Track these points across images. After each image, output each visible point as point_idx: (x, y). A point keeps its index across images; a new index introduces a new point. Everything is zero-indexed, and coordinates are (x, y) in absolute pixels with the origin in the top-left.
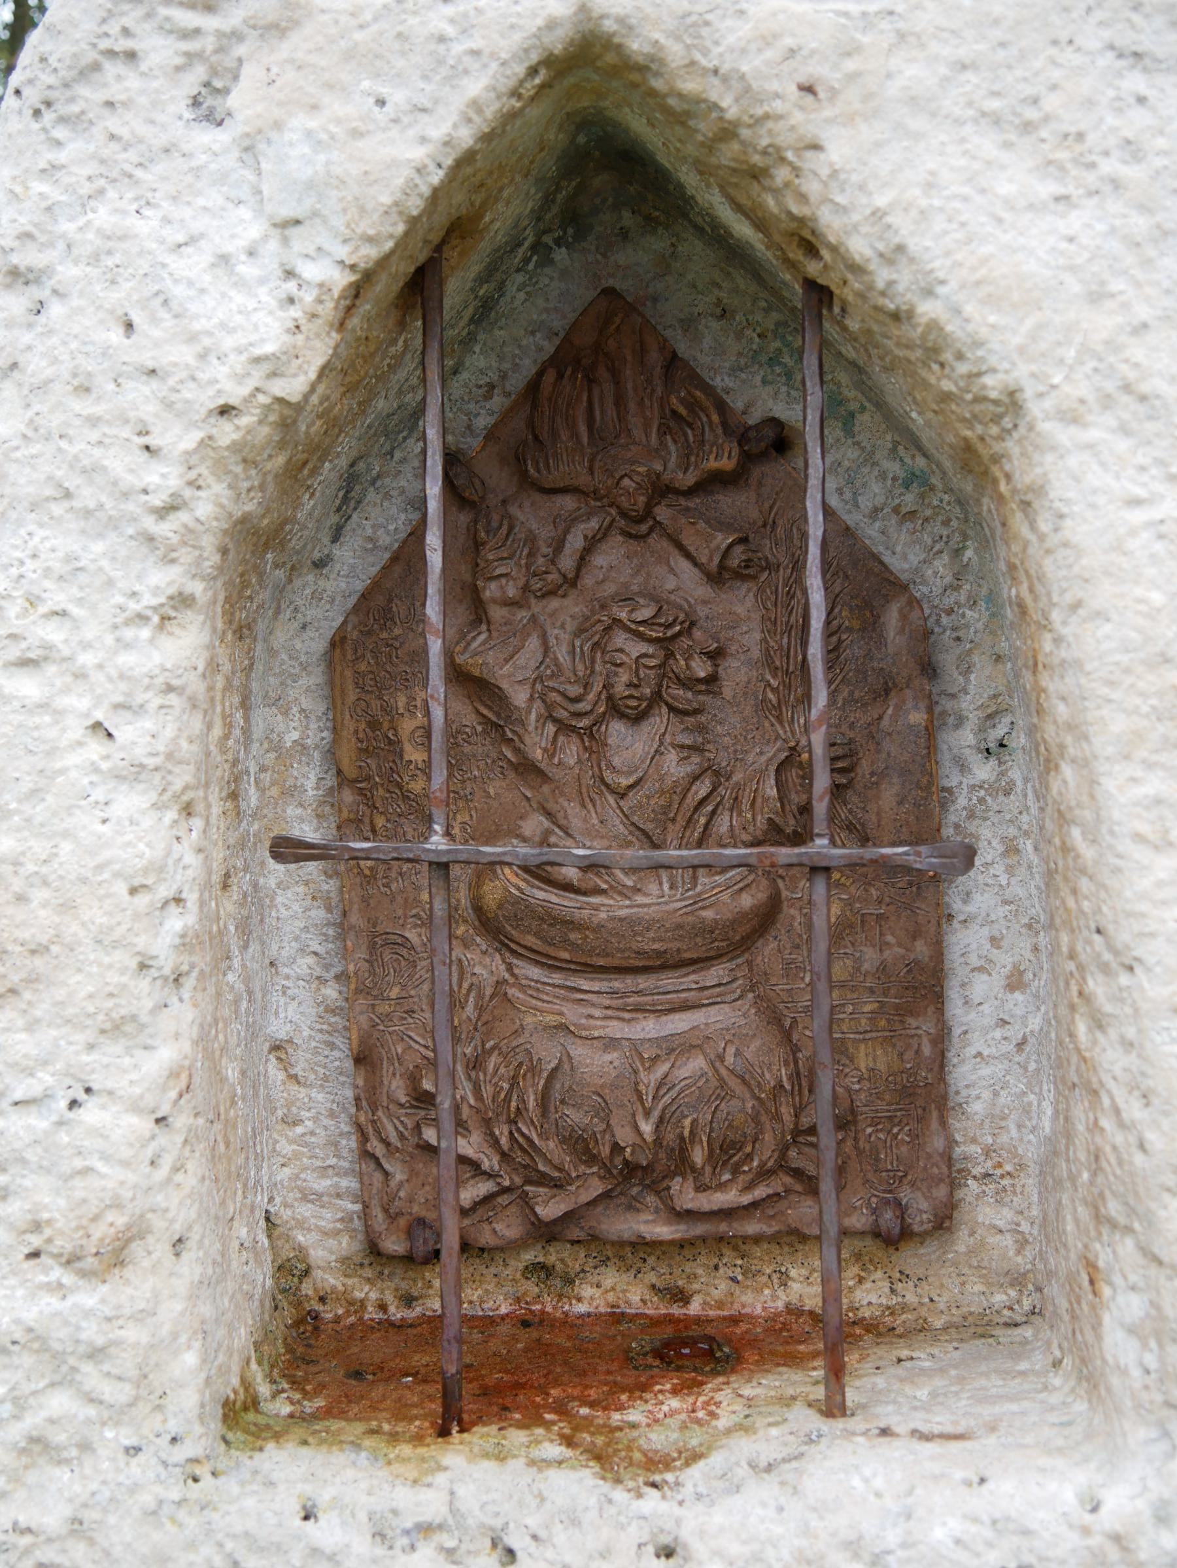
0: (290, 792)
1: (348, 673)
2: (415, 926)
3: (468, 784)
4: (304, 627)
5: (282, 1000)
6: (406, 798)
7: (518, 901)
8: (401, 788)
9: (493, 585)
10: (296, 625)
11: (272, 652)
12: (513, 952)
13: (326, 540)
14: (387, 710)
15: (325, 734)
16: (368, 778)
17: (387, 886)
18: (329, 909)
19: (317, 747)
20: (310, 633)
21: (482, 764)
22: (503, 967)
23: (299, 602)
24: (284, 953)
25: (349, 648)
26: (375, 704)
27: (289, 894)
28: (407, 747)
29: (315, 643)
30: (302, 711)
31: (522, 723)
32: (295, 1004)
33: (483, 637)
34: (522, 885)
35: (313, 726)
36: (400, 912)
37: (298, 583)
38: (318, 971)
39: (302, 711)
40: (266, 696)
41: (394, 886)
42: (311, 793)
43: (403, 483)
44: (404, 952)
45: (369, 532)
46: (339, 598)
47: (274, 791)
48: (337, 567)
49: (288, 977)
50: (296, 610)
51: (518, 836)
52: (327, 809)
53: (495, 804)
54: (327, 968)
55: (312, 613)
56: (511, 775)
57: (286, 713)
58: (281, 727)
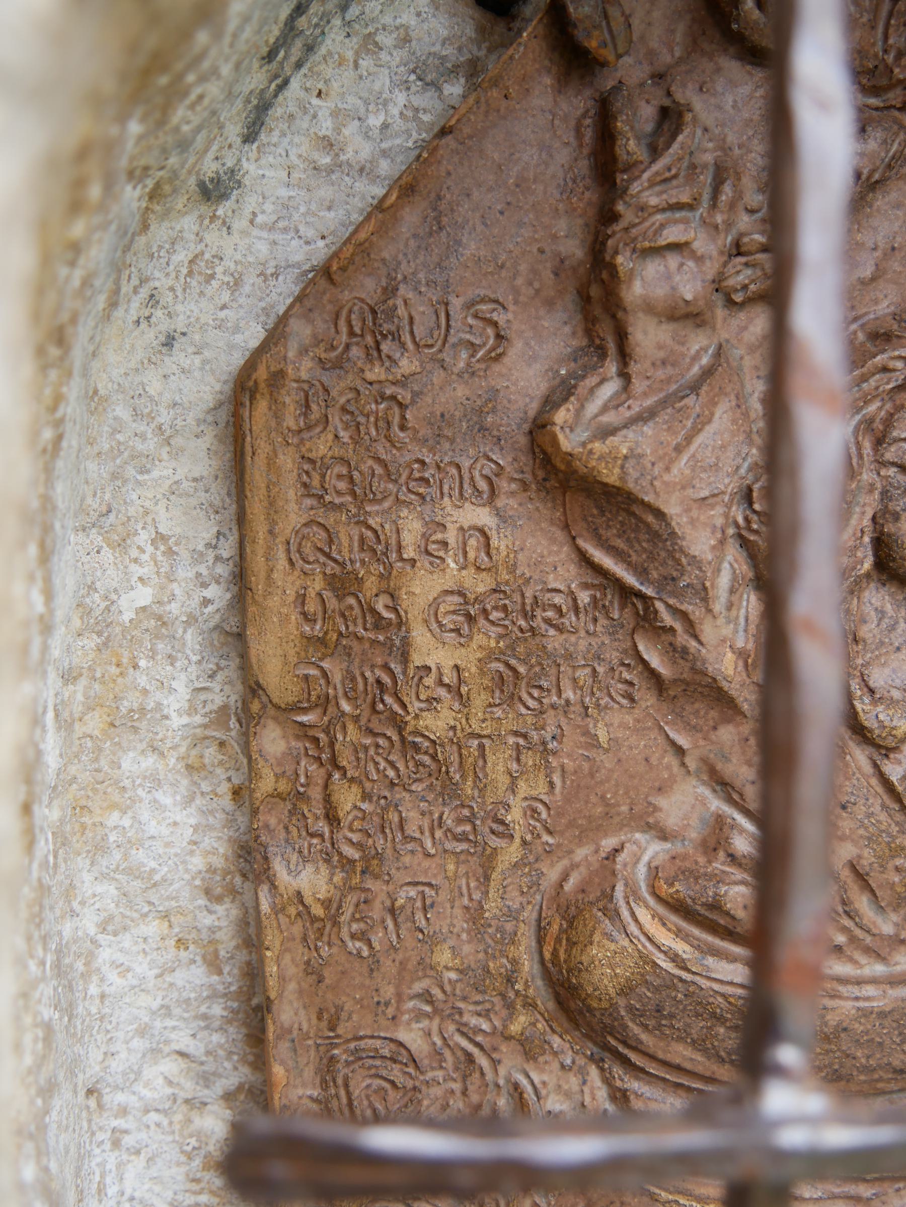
0: (126, 722)
1: (287, 461)
2: (419, 1015)
3: (550, 718)
4: (169, 342)
5: (112, 1159)
6: (408, 747)
7: (671, 982)
8: (400, 725)
9: (652, 268)
10: (151, 336)
11: (94, 399)
12: (626, 1062)
13: (234, 131)
14: (380, 549)
15: (214, 591)
16: (325, 703)
17: (361, 936)
18: (213, 964)
19: (191, 620)
20: (181, 357)
21: (583, 674)
22: (602, 1093)
23: (161, 282)
24: (116, 1065)
25: (290, 399)
26: (348, 537)
27: (127, 940)
28: (420, 636)
29: (195, 383)
30: (160, 538)
31: (704, 594)
32: (139, 1162)
33: (609, 389)
34: (681, 947)
35: (185, 572)
36: (389, 992)
37: (160, 232)
38: (189, 1088)
39: (160, 538)
40: (82, 510)
41: (377, 938)
42: (177, 721)
43: (407, 18)
44: (396, 1073)
45: (326, 126)
46: (251, 280)
47: (94, 723)
48: (251, 202)
49: (123, 1111)
50: (153, 299)
51: (648, 827)
52: (211, 753)
53: (607, 761)
54: (206, 1079)
55: (191, 310)
56: (647, 699)
57: (121, 545)
58: (110, 578)
